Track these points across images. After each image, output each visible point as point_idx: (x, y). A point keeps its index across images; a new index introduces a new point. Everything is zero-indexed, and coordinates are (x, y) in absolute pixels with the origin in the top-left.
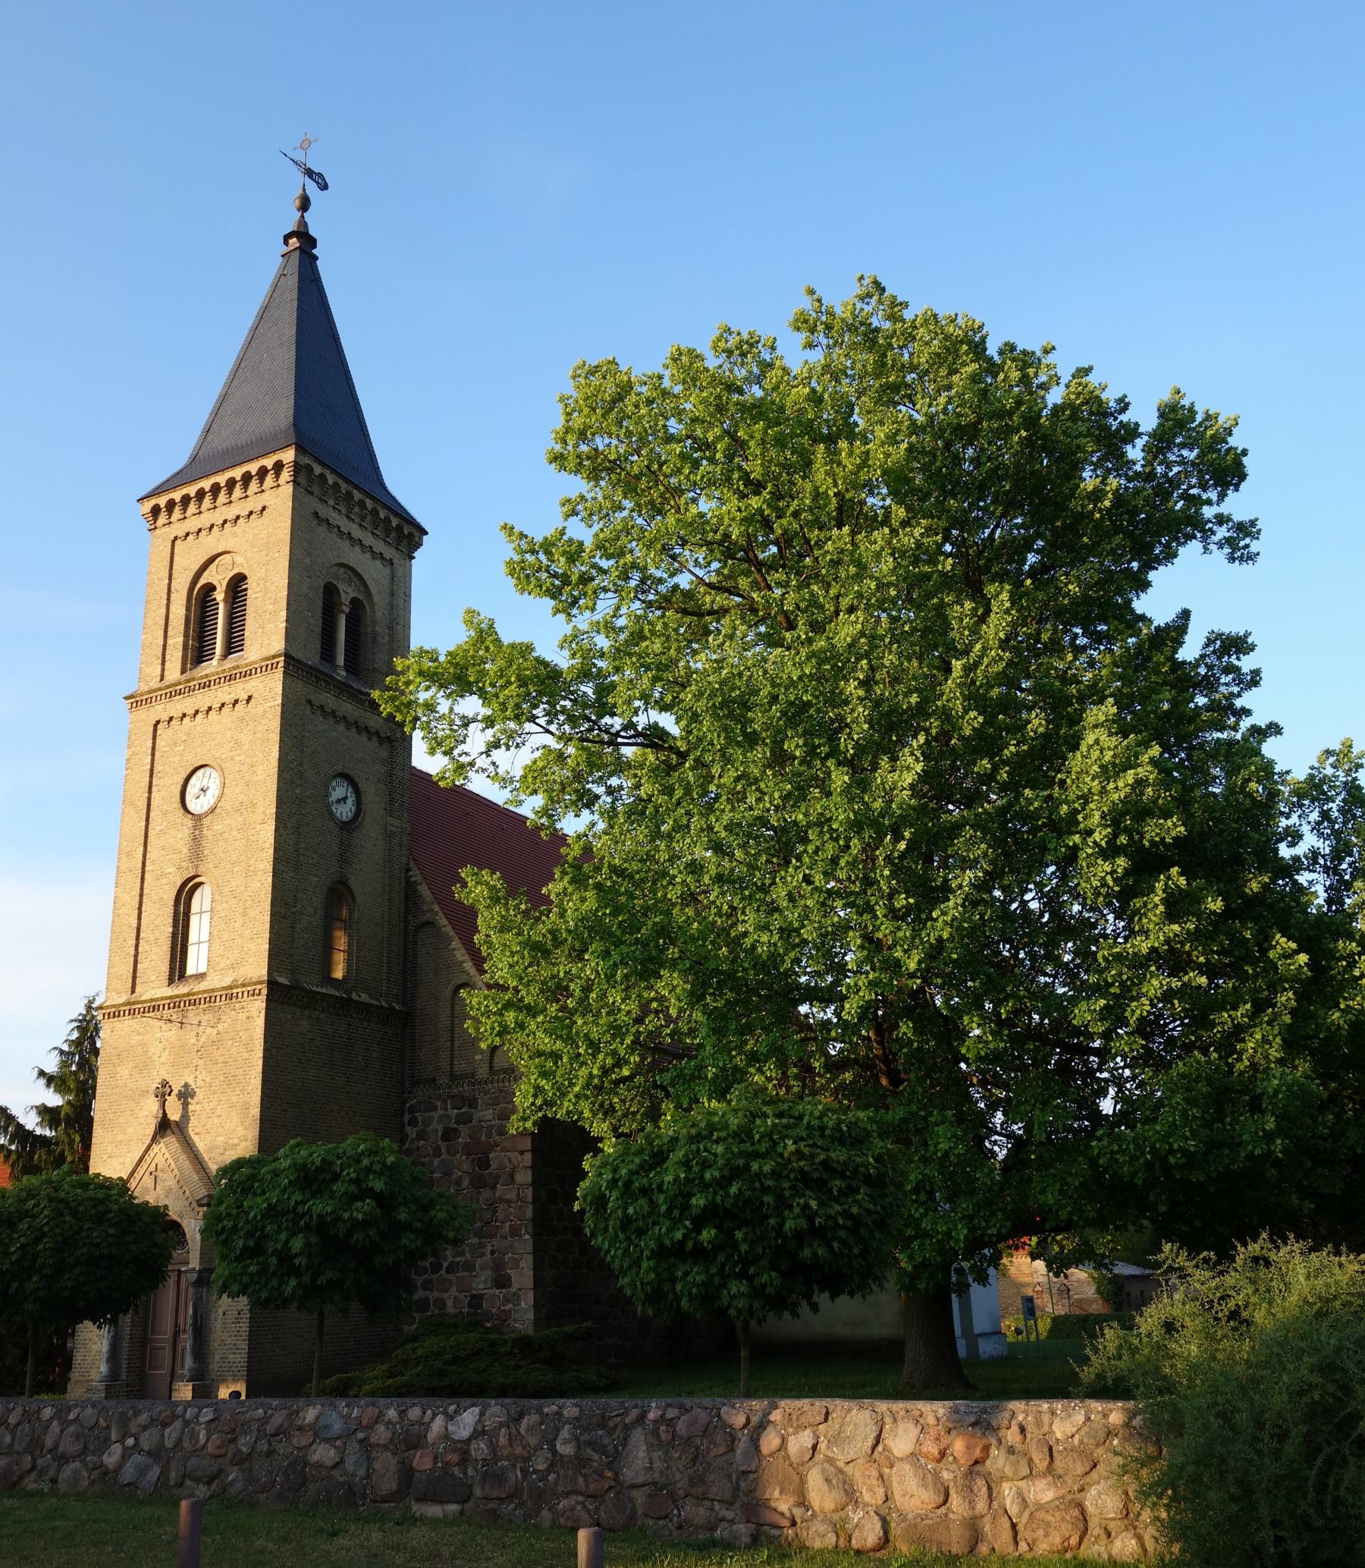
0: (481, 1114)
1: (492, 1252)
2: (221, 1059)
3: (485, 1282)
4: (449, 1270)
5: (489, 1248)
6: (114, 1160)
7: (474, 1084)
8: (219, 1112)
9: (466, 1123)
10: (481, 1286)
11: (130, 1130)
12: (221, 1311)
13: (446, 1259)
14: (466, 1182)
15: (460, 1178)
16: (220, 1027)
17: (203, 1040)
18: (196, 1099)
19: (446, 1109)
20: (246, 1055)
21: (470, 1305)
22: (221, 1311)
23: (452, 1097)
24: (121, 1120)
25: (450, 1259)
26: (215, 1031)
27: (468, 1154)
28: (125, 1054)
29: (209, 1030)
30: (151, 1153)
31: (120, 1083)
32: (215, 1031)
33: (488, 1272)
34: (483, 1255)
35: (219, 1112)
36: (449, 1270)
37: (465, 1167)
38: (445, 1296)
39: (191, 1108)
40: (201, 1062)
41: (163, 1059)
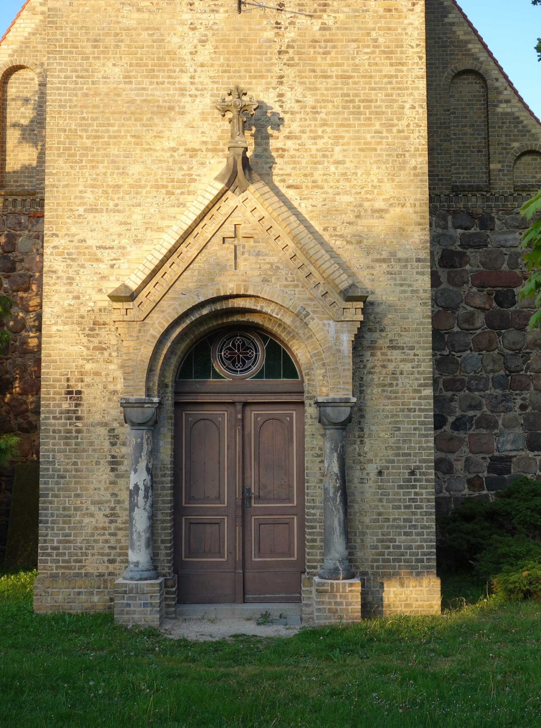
0: (501, 238)
1: (523, 407)
2: (335, 71)
3: (514, 442)
4: (456, 426)
5: (519, 402)
6: (104, 218)
7: (488, 199)
8: (338, 154)
9: (479, 247)
10: (509, 447)
11: (135, 169)
12: (372, 469)
13: (452, 412)
14: (480, 320)
15: (472, 314)
16: (328, 19)
17: (290, 35)
18: (285, 130)
19: (445, 227)
20: (388, 70)
21: (491, 469)
22: (372, 469)
23: (455, 213)
24: (113, 150)
25: (458, 413)
26: (316, 25)
27: (482, 287)
28: (110, 41)
29: (302, 20)
30: (225, 207)
31: (103, 88)
32: (316, 25)
33: (519, 430)
34: (508, 410)
35: (338, 154)
36: (456, 426)
37: (478, 301)
38: (451, 457)
39: (273, 144)
40: (290, 72)
41: (200, 59)
